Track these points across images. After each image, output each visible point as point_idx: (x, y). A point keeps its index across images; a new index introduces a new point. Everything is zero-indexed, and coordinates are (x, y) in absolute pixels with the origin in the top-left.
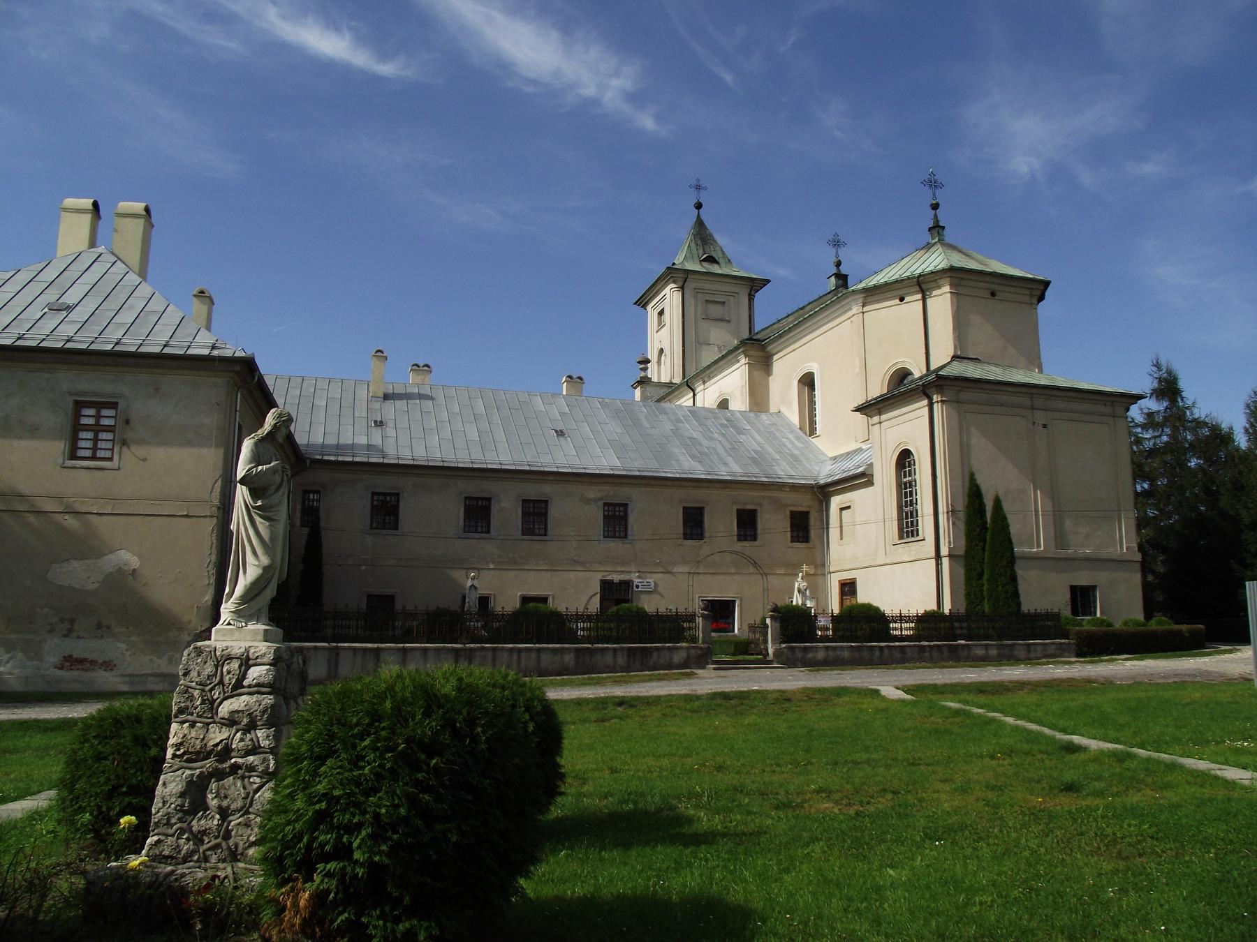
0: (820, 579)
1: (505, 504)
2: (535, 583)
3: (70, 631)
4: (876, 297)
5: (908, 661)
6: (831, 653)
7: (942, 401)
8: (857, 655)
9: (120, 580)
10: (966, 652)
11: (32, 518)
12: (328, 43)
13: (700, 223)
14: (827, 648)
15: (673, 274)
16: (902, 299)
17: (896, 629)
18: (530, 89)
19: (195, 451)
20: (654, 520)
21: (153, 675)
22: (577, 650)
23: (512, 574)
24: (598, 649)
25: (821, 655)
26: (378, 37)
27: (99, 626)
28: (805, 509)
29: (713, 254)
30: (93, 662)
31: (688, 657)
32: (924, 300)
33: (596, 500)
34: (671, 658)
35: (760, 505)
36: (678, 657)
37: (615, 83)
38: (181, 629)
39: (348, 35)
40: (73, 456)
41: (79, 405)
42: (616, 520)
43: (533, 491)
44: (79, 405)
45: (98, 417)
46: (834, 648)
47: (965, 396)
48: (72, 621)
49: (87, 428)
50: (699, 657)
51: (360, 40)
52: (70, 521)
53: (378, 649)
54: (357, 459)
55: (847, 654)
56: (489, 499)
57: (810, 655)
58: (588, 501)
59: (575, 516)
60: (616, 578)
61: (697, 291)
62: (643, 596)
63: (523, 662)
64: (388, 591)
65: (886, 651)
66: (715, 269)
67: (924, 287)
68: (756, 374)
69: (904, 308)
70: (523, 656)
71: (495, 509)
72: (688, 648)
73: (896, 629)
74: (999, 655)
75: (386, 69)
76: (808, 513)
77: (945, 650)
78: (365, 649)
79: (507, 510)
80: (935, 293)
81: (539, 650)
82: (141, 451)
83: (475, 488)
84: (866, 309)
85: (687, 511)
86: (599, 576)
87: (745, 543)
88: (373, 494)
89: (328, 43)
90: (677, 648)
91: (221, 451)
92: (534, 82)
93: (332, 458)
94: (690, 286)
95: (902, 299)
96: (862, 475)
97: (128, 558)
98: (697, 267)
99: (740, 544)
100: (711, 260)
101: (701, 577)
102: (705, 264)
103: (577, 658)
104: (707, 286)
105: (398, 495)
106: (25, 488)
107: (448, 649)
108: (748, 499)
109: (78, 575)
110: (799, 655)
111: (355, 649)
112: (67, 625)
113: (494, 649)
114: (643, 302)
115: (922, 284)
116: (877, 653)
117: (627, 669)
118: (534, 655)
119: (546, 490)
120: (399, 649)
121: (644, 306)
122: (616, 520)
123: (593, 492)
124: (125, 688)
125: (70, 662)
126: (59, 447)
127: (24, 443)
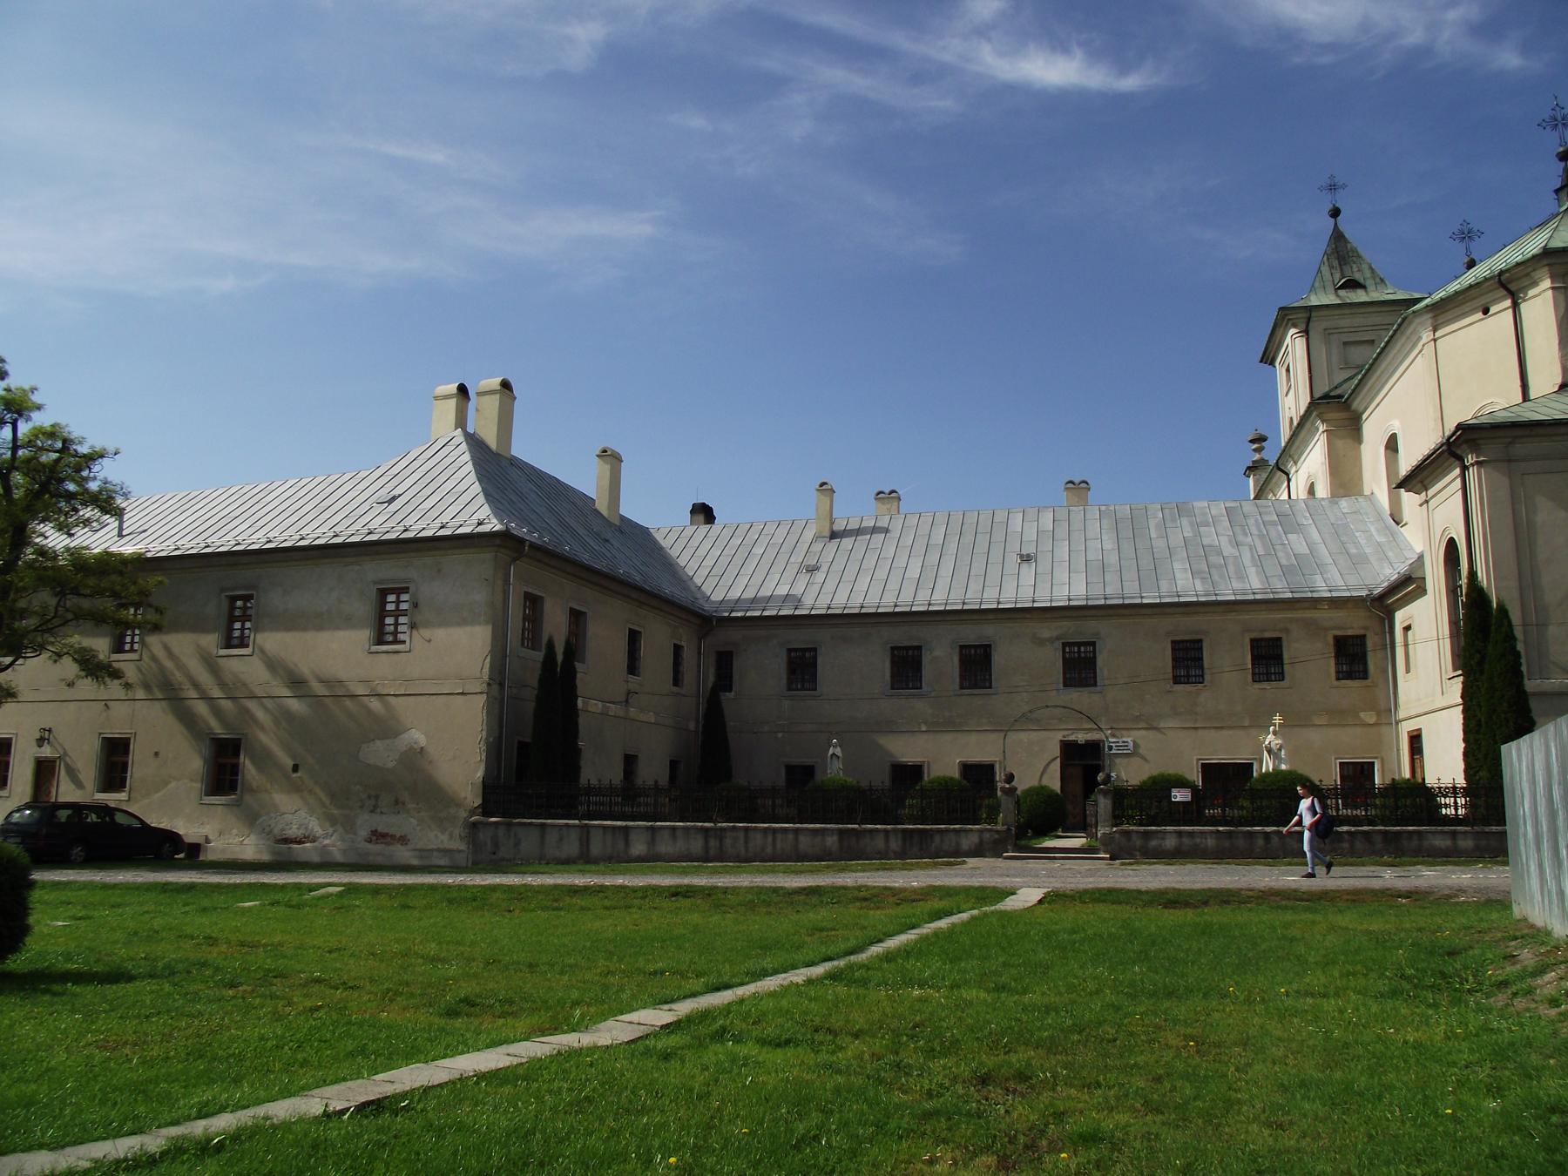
0: (1384, 729)
1: (937, 653)
2: (980, 748)
3: (375, 807)
4: (1449, 315)
5: (595, 861)
6: (1186, 840)
7: (1477, 463)
8: (1227, 844)
9: (414, 758)
10: (1415, 843)
11: (348, 703)
12: (1054, 70)
13: (1338, 237)
14: (1180, 833)
15: (1286, 317)
16: (1486, 311)
17: (1446, 806)
18: (1326, 59)
19: (468, 629)
20: (1130, 661)
21: (439, 850)
22: (841, 832)
23: (948, 737)
24: (866, 831)
25: (1170, 843)
26: (1116, 49)
27: (397, 802)
28: (1361, 632)
29: (1358, 276)
30: (393, 837)
31: (981, 842)
32: (1515, 306)
33: (1052, 640)
34: (958, 844)
35: (1287, 631)
36: (967, 842)
37: (1452, 15)
38: (458, 805)
39: (1079, 53)
40: (380, 642)
41: (383, 593)
42: (1080, 667)
43: (972, 634)
44: (383, 593)
45: (398, 602)
46: (1191, 834)
47: (1519, 449)
48: (377, 797)
49: (390, 613)
50: (996, 842)
51: (1095, 55)
52: (375, 704)
53: (627, 827)
54: (766, 613)
55: (1211, 842)
56: (919, 648)
57: (1154, 843)
58: (1041, 642)
59: (1026, 663)
60: (1081, 737)
61: (1328, 333)
62: (1118, 761)
63: (779, 845)
64: (808, 761)
65: (1275, 840)
66: (1359, 296)
67: (1513, 287)
68: (1340, 443)
69: (1490, 321)
70: (779, 836)
71: (926, 659)
72: (981, 831)
73: (1446, 806)
74: (1477, 848)
75: (1130, 83)
76: (1364, 636)
77: (1378, 839)
78: (614, 828)
79: (941, 660)
80: (1531, 293)
81: (797, 830)
82: (426, 633)
83: (902, 636)
84: (1438, 334)
85: (1177, 646)
86: (1059, 736)
87: (1265, 685)
88: (790, 650)
89: (1054, 70)
90: (966, 831)
91: (490, 628)
92: (1332, 47)
93: (757, 613)
94: (1317, 327)
95: (1486, 311)
96: (1406, 580)
97: (417, 736)
98: (1329, 299)
99: (1257, 686)
100: (1352, 284)
101: (1200, 732)
102: (1342, 293)
103: (841, 840)
104: (1342, 323)
105: (815, 650)
106: (342, 674)
107: (696, 828)
108: (1267, 625)
109: (381, 754)
110: (1138, 843)
111: (604, 827)
112: (373, 802)
113: (746, 829)
114: (1268, 358)
115: (1510, 285)
116: (1261, 842)
117: (902, 855)
118: (791, 836)
119: (988, 631)
120: (648, 828)
121: (1272, 363)
122: (1080, 667)
123: (1047, 631)
124: (415, 862)
125: (377, 836)
126: (364, 635)
127: (341, 634)
